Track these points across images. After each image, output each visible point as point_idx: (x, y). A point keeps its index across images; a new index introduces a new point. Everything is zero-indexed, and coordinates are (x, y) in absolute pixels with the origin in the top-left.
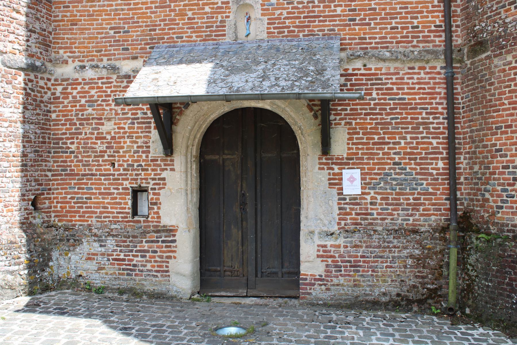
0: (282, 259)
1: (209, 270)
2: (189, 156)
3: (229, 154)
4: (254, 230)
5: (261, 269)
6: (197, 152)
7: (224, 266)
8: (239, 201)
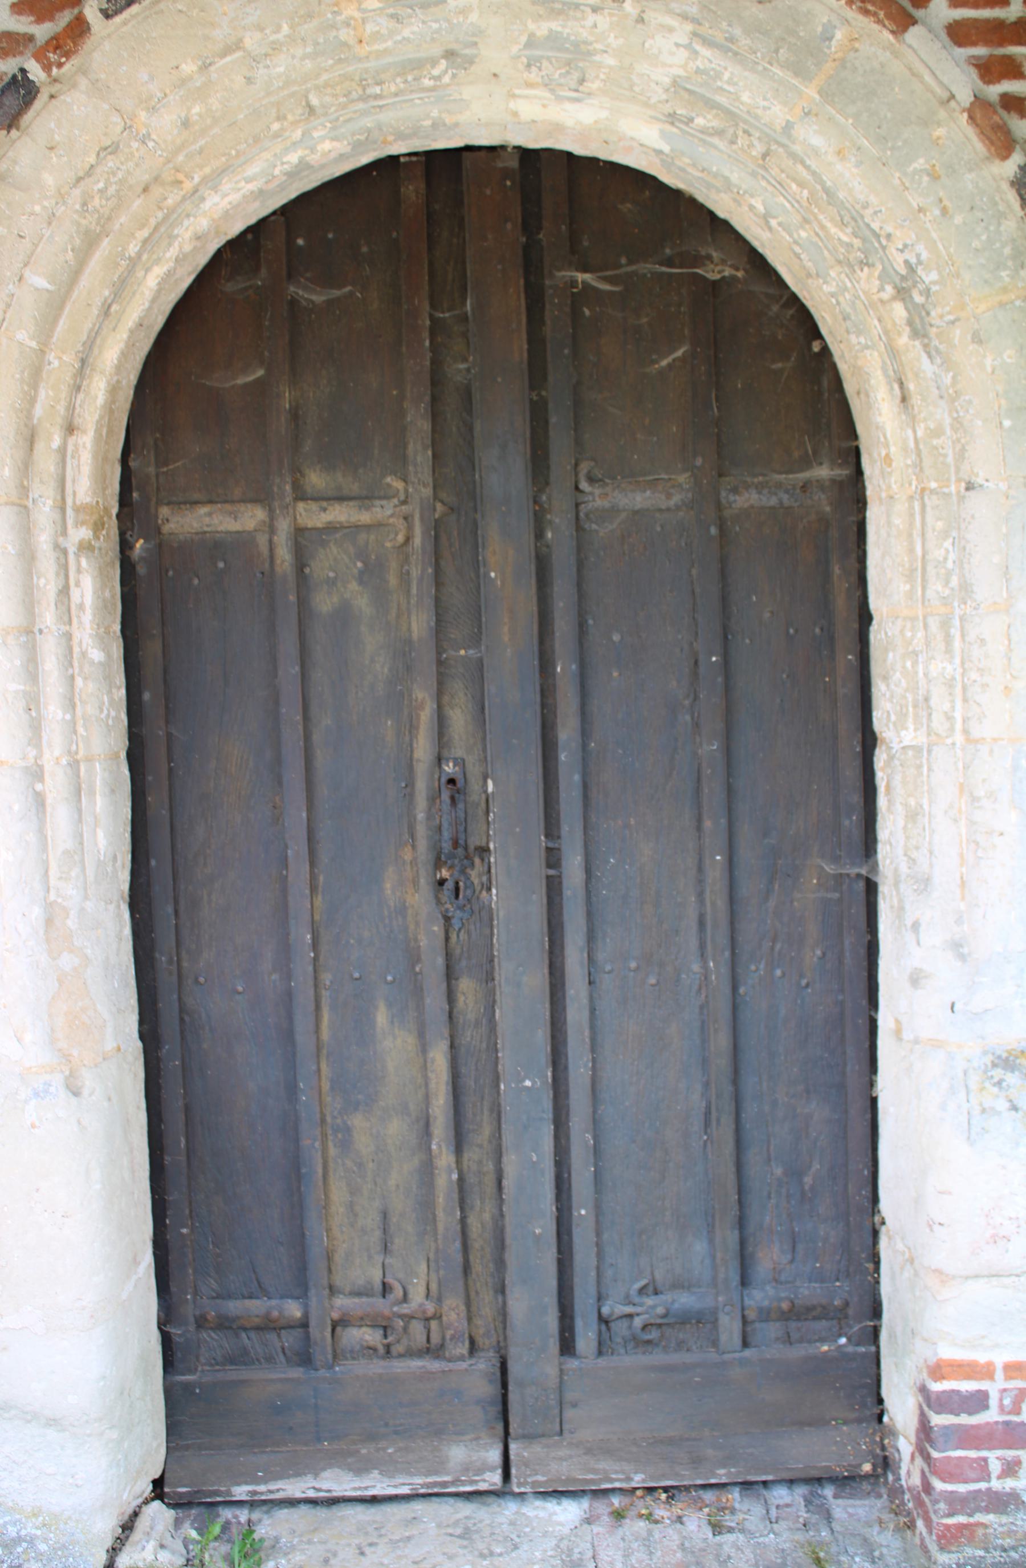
0: (741, 1223)
1: (225, 1324)
2: (45, 512)
3: (341, 499)
4: (542, 1036)
5: (600, 1298)
6: (100, 479)
7: (332, 1290)
8: (421, 831)
